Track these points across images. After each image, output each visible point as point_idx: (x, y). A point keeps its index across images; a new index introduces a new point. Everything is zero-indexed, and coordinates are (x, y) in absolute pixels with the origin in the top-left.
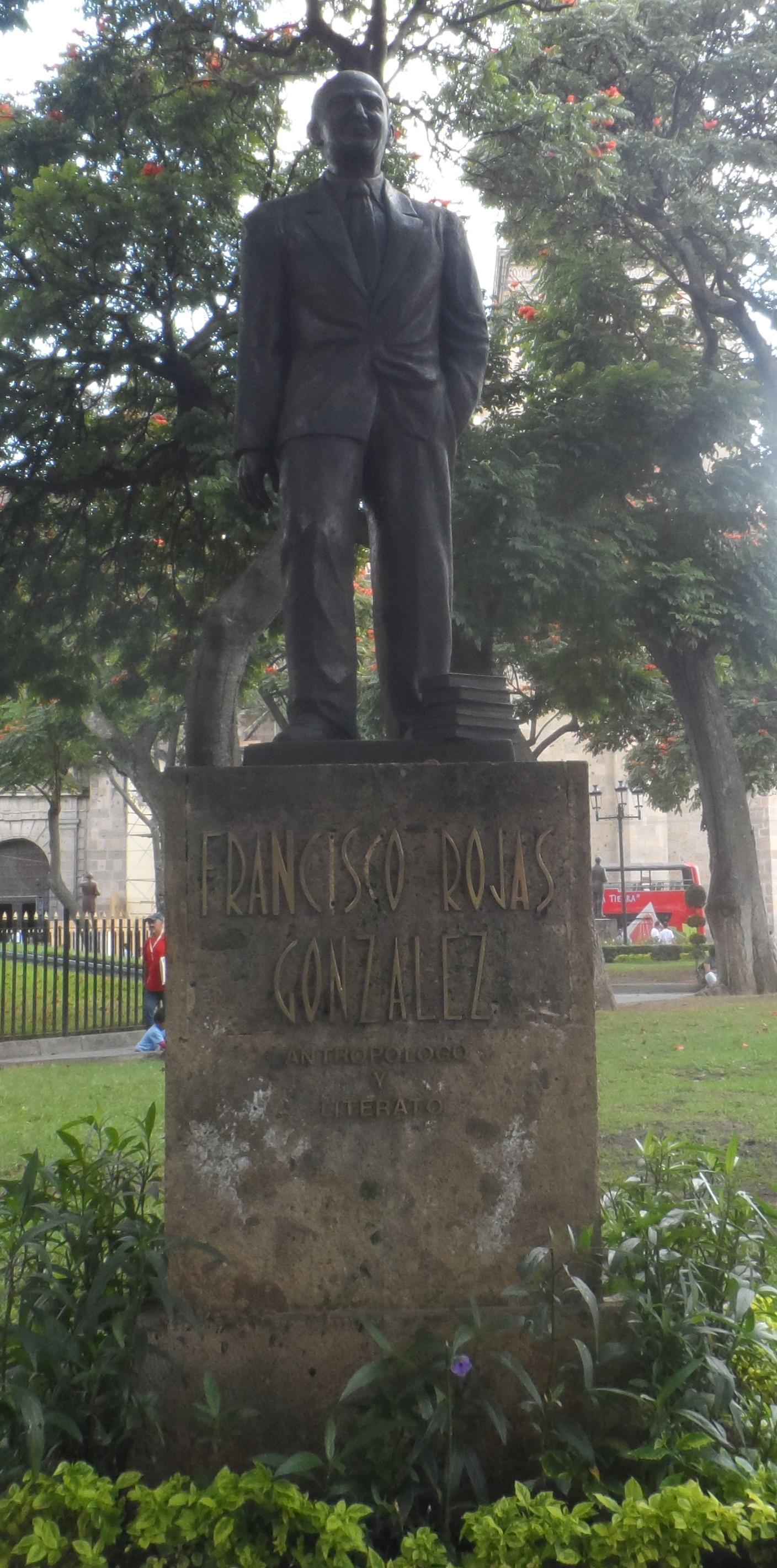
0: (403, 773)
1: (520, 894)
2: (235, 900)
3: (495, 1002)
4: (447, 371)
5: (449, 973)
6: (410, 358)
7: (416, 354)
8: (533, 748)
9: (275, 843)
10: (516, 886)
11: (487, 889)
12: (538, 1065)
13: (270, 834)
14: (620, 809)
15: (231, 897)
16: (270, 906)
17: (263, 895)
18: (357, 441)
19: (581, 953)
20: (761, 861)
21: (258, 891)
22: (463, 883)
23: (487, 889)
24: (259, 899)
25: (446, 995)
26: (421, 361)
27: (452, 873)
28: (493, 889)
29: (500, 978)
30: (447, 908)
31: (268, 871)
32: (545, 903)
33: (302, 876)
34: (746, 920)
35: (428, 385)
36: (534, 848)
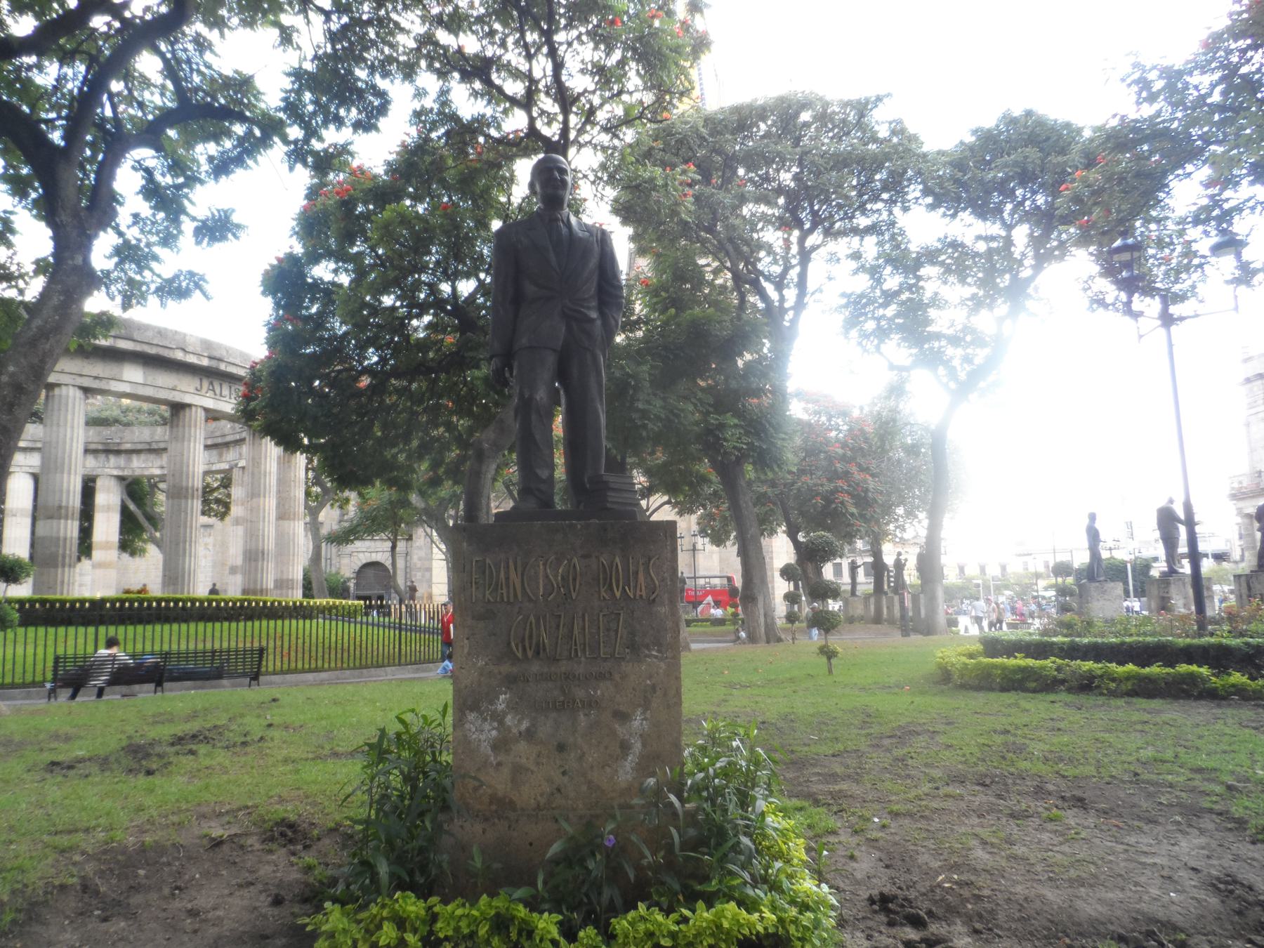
4: (602, 315)
9: (511, 564)
17: (504, 591)
18: (554, 350)
20: (769, 573)
22: (611, 584)
26: (589, 308)
27: (605, 579)
31: (507, 579)
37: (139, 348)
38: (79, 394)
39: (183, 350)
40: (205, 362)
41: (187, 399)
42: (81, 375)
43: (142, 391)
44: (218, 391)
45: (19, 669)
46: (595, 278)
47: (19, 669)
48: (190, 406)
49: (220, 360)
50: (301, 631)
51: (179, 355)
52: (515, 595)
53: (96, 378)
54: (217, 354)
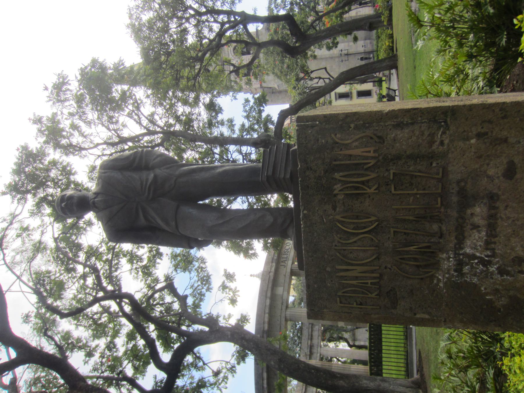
0: (305, 212)
1: (370, 152)
2: (370, 188)
3: (431, 164)
4: (153, 168)
5: (413, 190)
6: (146, 184)
7: (144, 183)
8: (331, 79)
9: (342, 274)
10: (365, 154)
11: (367, 169)
12: (473, 139)
13: (337, 276)
14: (346, 55)
15: (370, 295)
16: (375, 278)
17: (369, 281)
18: (178, 207)
19: (404, 115)
20: (358, 17)
21: (367, 283)
22: (363, 183)
23: (367, 169)
24: (371, 283)
25: (427, 192)
26: (147, 180)
27: (357, 188)
28: (365, 167)
29: (418, 162)
30: (377, 191)
31: (357, 278)
32: (374, 137)
33: (359, 262)
34: (374, 20)
35: (155, 177)
36: (343, 144)
37: (270, 289)
38: (288, 310)
39: (270, 272)
40: (274, 264)
41: (289, 270)
42: (282, 309)
43: (286, 288)
44: (285, 259)
45: (399, 333)
46: (128, 174)
47: (399, 333)
48: (291, 270)
49: (273, 259)
50: (395, 333)
51: (272, 274)
52: (372, 272)
53: (282, 304)
54: (271, 260)
